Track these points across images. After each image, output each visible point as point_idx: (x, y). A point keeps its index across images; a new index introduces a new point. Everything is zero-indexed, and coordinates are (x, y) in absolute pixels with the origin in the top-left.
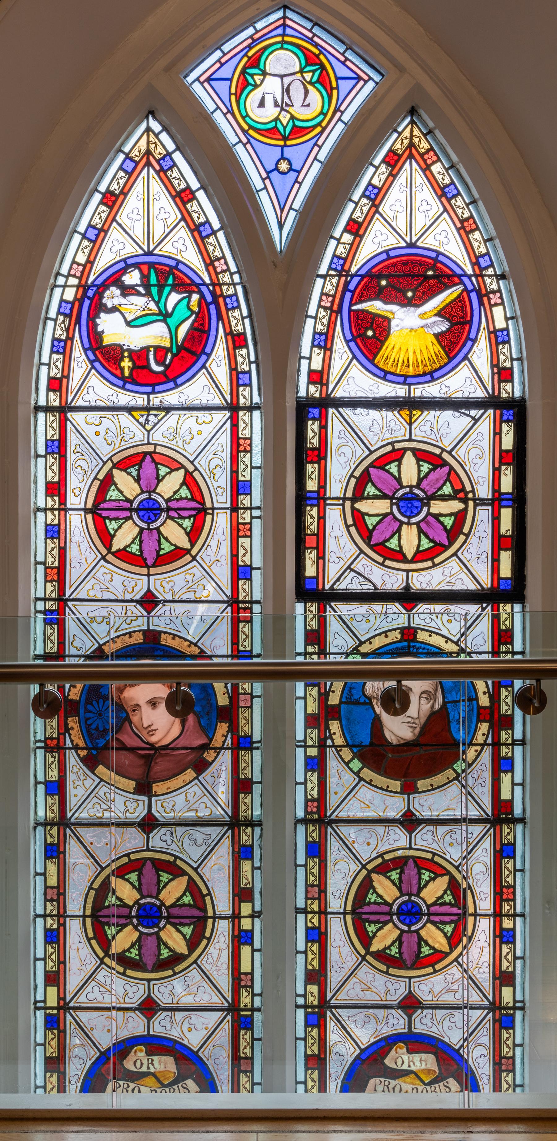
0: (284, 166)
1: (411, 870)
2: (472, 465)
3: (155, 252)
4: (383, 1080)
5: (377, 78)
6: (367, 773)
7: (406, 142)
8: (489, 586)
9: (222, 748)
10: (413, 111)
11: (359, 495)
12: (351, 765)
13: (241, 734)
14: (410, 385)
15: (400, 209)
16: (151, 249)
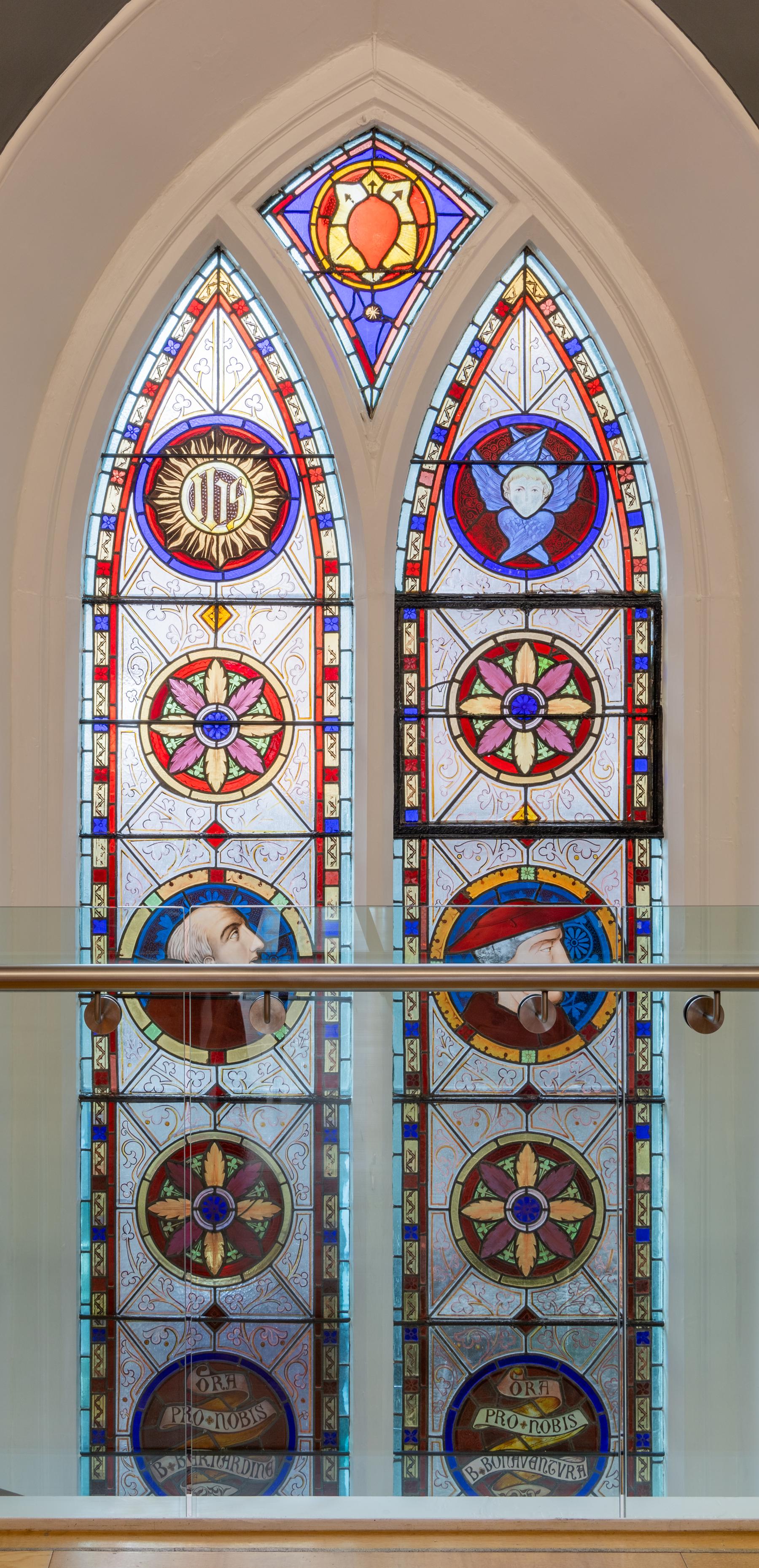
1: (566, 1173)
2: (291, 678)
6: (166, 1041)
7: (213, 289)
8: (621, 818)
11: (585, 720)
15: (206, 370)
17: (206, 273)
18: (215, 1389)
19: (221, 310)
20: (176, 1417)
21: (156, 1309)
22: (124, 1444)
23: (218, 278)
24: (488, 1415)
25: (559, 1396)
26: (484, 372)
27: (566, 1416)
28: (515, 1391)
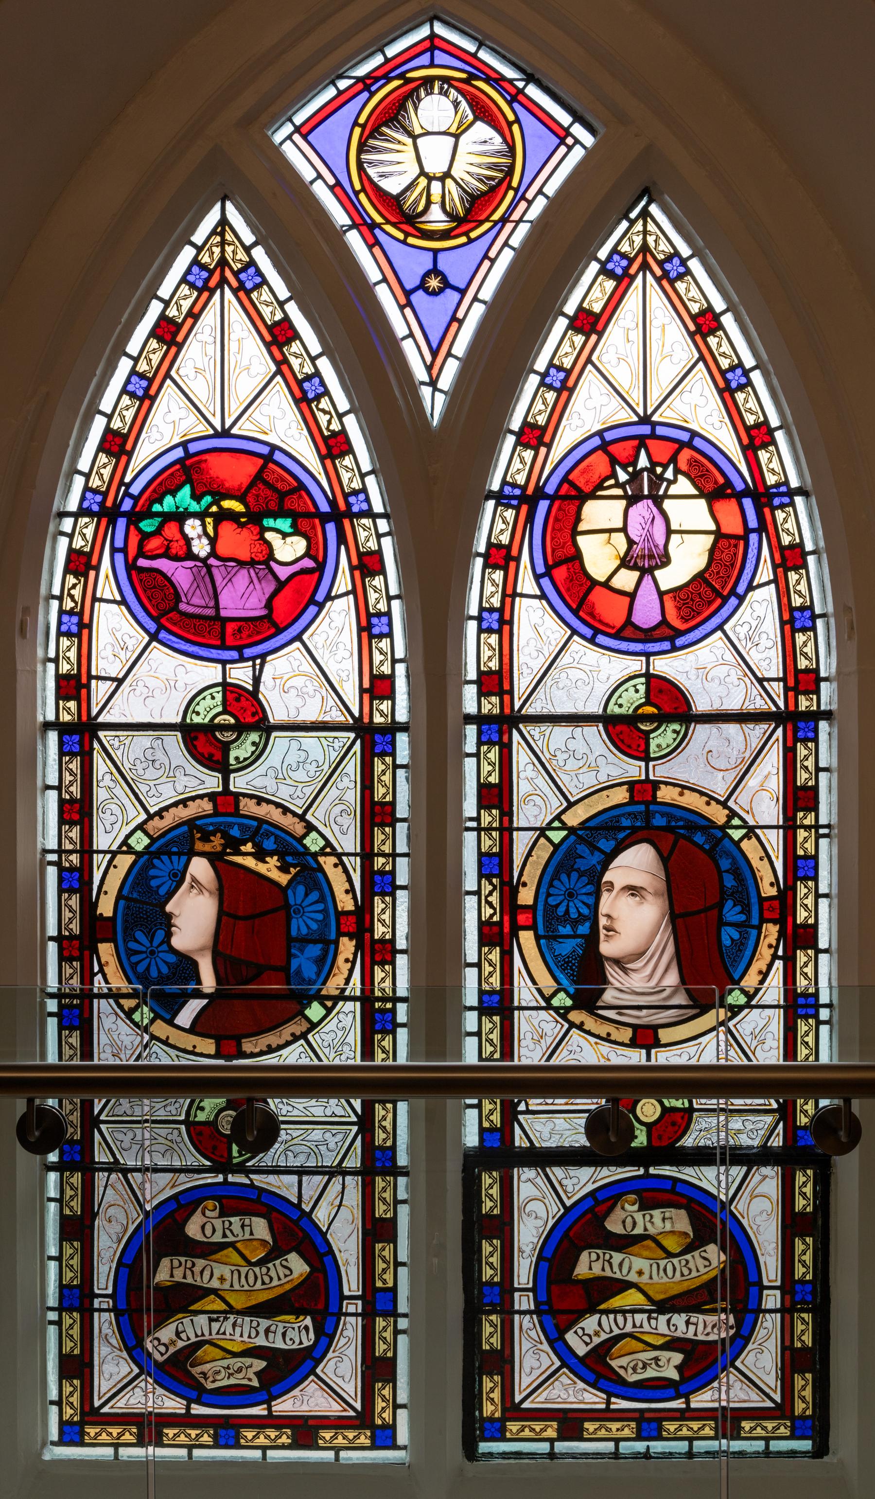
3: (234, 431)
5: (588, 139)
19: (649, 276)
20: (175, 1272)
21: (557, 1128)
22: (523, 1302)
24: (172, 1268)
25: (268, 1238)
26: (168, 375)
27: (277, 1262)
28: (208, 1232)
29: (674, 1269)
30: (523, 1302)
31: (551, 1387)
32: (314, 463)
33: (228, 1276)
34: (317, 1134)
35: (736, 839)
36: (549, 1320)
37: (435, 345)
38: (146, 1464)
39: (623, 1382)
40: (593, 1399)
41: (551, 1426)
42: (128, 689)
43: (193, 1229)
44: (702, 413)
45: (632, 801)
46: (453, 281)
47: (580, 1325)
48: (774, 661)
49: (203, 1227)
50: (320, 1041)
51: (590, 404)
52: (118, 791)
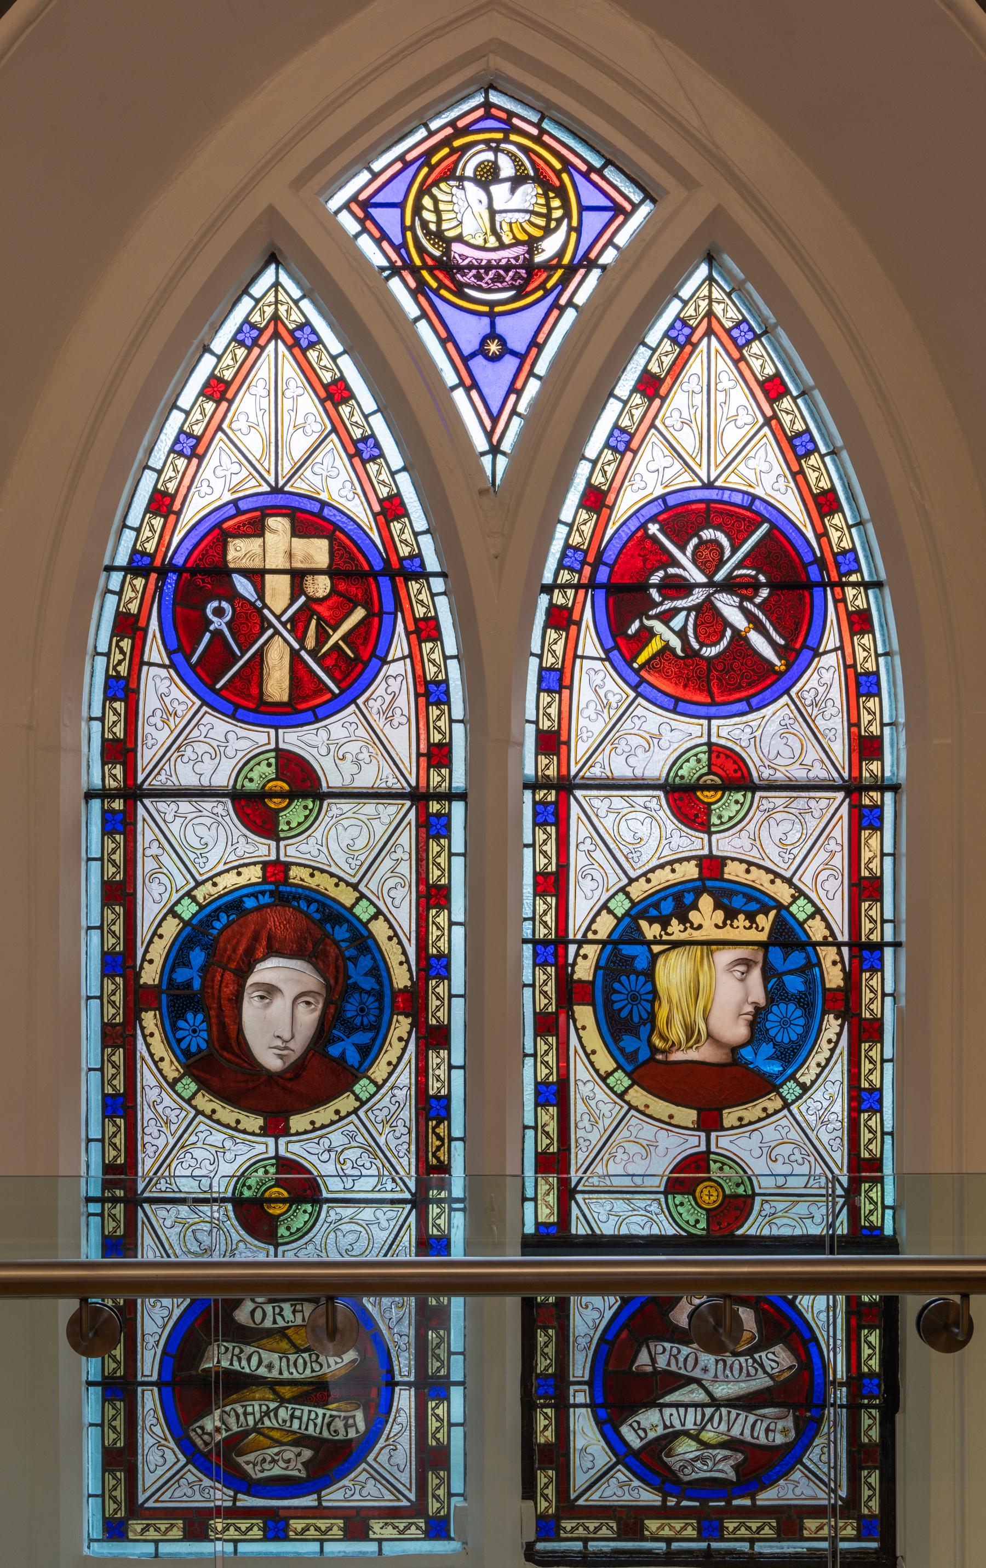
0: (494, 347)
4: (668, 1345)
7: (269, 311)
9: (580, 943)
10: (710, 259)
12: (810, 909)
13: (551, 970)
14: (639, 695)
16: (712, 479)
17: (257, 290)
18: (275, 1322)
19: (280, 342)
22: (579, 1396)
23: (276, 296)
29: (305, 1363)
30: (579, 1396)
31: (176, 1485)
32: (799, 515)
33: (276, 1363)
34: (367, 1213)
35: (365, 920)
36: (602, 1412)
37: (495, 411)
38: (115, 1560)
39: (678, 1482)
40: (221, 1496)
41: (691, 1524)
42: (609, 748)
43: (242, 1315)
44: (768, 480)
45: (265, 880)
46: (511, 344)
47: (637, 1418)
48: (840, 731)
49: (252, 1313)
50: (372, 1118)
51: (652, 467)
52: (597, 855)
